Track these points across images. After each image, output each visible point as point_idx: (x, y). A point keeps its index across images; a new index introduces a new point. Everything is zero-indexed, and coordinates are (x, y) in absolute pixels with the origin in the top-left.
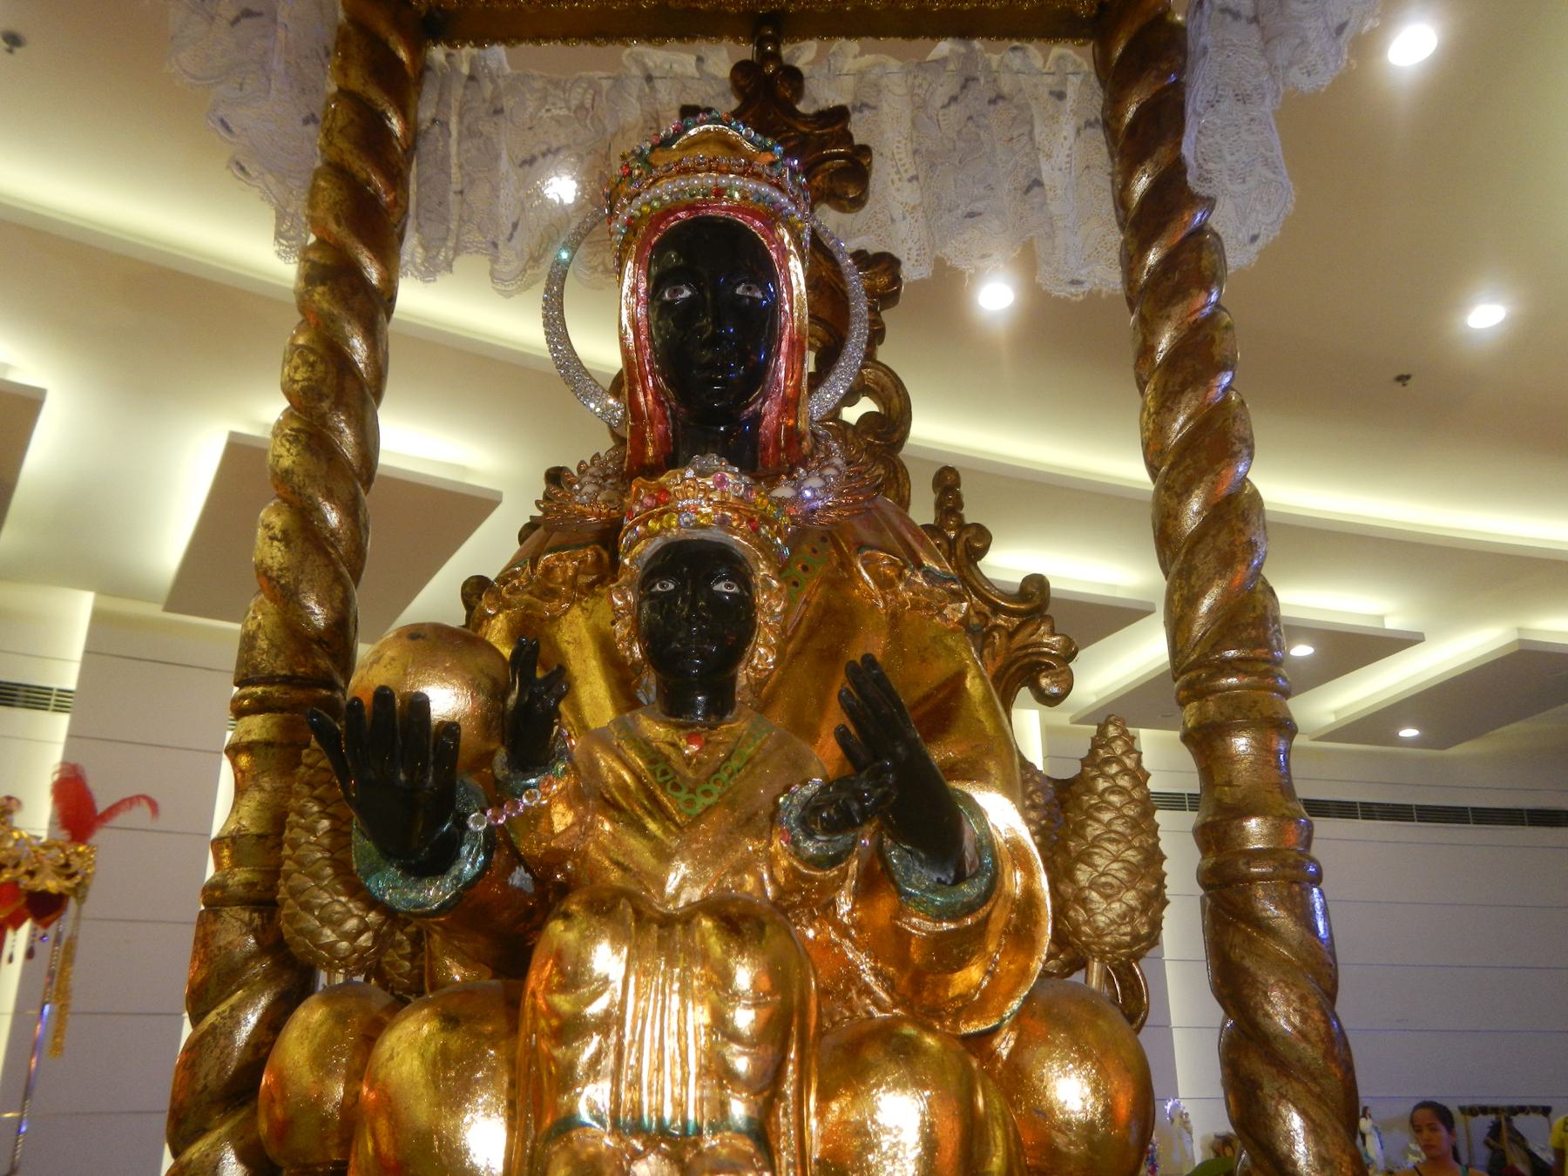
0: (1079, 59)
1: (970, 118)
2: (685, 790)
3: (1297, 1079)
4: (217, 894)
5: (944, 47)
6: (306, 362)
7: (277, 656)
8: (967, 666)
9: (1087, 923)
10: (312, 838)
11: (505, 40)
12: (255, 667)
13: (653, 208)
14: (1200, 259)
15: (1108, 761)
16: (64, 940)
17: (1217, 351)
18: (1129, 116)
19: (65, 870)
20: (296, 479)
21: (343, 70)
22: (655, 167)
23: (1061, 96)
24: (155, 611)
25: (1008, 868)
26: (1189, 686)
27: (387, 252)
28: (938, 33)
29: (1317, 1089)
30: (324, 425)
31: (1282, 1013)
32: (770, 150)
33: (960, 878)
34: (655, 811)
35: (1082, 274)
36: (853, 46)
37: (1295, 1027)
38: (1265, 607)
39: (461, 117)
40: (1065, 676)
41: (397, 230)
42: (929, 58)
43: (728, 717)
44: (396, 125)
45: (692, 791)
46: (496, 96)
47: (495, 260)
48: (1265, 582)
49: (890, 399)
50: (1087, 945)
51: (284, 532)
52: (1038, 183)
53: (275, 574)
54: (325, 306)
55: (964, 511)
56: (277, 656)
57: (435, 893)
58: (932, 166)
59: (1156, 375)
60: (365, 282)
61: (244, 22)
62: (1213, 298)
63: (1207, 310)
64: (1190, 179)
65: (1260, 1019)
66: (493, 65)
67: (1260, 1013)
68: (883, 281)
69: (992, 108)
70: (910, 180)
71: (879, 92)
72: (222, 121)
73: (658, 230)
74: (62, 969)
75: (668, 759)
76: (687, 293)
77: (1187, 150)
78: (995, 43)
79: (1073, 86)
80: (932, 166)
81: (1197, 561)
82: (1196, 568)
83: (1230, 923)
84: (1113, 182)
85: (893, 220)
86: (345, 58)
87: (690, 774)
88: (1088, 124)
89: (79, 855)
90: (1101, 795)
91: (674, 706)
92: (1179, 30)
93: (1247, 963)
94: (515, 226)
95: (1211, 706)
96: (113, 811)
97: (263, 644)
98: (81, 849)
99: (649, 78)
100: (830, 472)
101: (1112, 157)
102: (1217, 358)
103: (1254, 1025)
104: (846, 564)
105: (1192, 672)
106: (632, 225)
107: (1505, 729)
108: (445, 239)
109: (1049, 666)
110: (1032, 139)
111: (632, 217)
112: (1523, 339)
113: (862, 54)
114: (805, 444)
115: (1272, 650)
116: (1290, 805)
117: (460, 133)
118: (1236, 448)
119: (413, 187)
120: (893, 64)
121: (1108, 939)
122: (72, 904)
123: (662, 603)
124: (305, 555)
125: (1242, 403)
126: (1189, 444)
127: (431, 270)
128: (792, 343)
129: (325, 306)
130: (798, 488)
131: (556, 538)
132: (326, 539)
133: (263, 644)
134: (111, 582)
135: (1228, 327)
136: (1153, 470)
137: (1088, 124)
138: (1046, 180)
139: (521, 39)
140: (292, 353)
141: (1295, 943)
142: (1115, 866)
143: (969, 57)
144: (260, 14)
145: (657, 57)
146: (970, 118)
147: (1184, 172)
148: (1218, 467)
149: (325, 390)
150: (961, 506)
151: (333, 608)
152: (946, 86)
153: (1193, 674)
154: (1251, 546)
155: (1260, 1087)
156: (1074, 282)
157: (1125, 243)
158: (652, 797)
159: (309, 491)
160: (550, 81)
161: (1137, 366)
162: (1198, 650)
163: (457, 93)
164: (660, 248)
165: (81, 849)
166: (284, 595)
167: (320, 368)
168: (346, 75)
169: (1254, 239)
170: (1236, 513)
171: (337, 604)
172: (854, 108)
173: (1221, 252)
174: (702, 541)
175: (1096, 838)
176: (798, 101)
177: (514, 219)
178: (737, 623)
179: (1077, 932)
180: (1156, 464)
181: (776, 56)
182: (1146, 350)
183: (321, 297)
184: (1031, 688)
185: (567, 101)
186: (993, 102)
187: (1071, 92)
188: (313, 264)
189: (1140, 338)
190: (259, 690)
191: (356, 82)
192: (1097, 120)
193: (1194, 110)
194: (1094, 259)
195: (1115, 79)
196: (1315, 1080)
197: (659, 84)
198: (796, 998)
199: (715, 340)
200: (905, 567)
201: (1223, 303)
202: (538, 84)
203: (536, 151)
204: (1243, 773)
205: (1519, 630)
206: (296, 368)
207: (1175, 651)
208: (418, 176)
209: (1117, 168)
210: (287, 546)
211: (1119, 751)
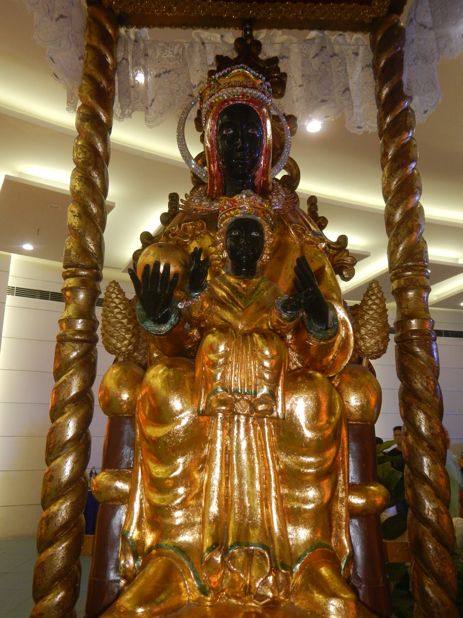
0: (364, 40)
1: (323, 63)
2: (244, 298)
3: (424, 403)
4: (63, 338)
5: (313, 34)
6: (83, 151)
7: (79, 257)
8: (326, 264)
9: (364, 345)
10: (113, 315)
11: (148, 26)
12: (71, 261)
13: (219, 99)
14: (406, 120)
15: (372, 295)
17: (411, 155)
18: (382, 64)
20: (82, 195)
21: (89, 36)
22: (220, 84)
23: (356, 54)
25: (341, 326)
26: (395, 274)
27: (109, 111)
28: (312, 29)
29: (430, 406)
30: (91, 175)
31: (419, 385)
33: (327, 328)
34: (234, 304)
35: (362, 125)
36: (280, 32)
37: (424, 386)
38: (423, 248)
39: (133, 57)
40: (352, 271)
42: (307, 38)
44: (109, 60)
45: (246, 298)
46: (145, 49)
47: (147, 113)
48: (423, 239)
49: (293, 170)
50: (363, 353)
51: (79, 214)
52: (348, 89)
53: (76, 229)
54: (89, 130)
55: (318, 212)
56: (79, 257)
57: (165, 328)
58: (309, 81)
59: (388, 164)
60: (102, 121)
61: (61, 20)
62: (410, 135)
63: (408, 139)
64: (405, 89)
66: (143, 36)
67: (413, 382)
69: (331, 58)
70: (300, 86)
71: (289, 51)
72: (51, 58)
75: (237, 288)
76: (231, 132)
77: (405, 78)
78: (332, 32)
79: (361, 50)
80: (309, 81)
81: (400, 231)
82: (399, 233)
83: (405, 354)
84: (375, 89)
85: (293, 102)
86: (90, 32)
87: (244, 293)
88: (367, 66)
90: (370, 306)
91: (237, 272)
92: (402, 30)
93: (410, 366)
94: (153, 101)
95: (402, 282)
97: (73, 253)
99: (203, 44)
100: (280, 196)
101: (375, 79)
102: (411, 157)
103: (411, 386)
104: (287, 229)
105: (396, 270)
108: (129, 106)
109: (346, 268)
110: (346, 72)
111: (212, 103)
113: (282, 35)
114: (270, 187)
115: (424, 262)
116: (427, 315)
117: (133, 63)
118: (416, 191)
120: (295, 40)
121: (370, 351)
123: (236, 239)
124: (86, 222)
125: (419, 174)
126: (399, 189)
128: (266, 151)
129: (89, 130)
131: (186, 218)
133: (73, 253)
135: (415, 146)
136: (386, 198)
137: (367, 66)
138: (351, 87)
139: (154, 26)
140: (77, 148)
141: (425, 360)
142: (373, 328)
143: (323, 39)
144: (66, 17)
145: (205, 34)
146: (323, 63)
147: (402, 86)
148: (410, 197)
149: (90, 162)
150: (317, 210)
151: (97, 241)
152: (314, 50)
153: (397, 271)
154: (419, 226)
155: (412, 406)
156: (359, 127)
157: (379, 114)
158: (233, 300)
159: (87, 199)
160: (166, 43)
161: (381, 160)
162: (399, 262)
163: (130, 47)
164: (221, 115)
166: (79, 236)
167: (88, 153)
168: (91, 39)
170: (414, 216)
171: (98, 240)
172: (280, 57)
173: (414, 116)
174: (247, 219)
175: (367, 319)
176: (259, 54)
177: (153, 98)
178: (257, 246)
179: (360, 349)
180: (387, 196)
181: (251, 36)
182: (385, 154)
183: (87, 126)
185: (172, 52)
186: (332, 56)
187: (360, 53)
188: (83, 114)
189: (383, 149)
191: (95, 42)
192: (370, 65)
193: (408, 64)
194: (365, 116)
195: (378, 48)
196: (429, 403)
197: (208, 47)
198: (284, 357)
199: (242, 149)
201: (414, 137)
202: (161, 44)
203: (161, 72)
204: (411, 304)
206: (79, 154)
207: (391, 262)
208: (118, 81)
209: (378, 84)
210: (80, 219)
211: (376, 292)
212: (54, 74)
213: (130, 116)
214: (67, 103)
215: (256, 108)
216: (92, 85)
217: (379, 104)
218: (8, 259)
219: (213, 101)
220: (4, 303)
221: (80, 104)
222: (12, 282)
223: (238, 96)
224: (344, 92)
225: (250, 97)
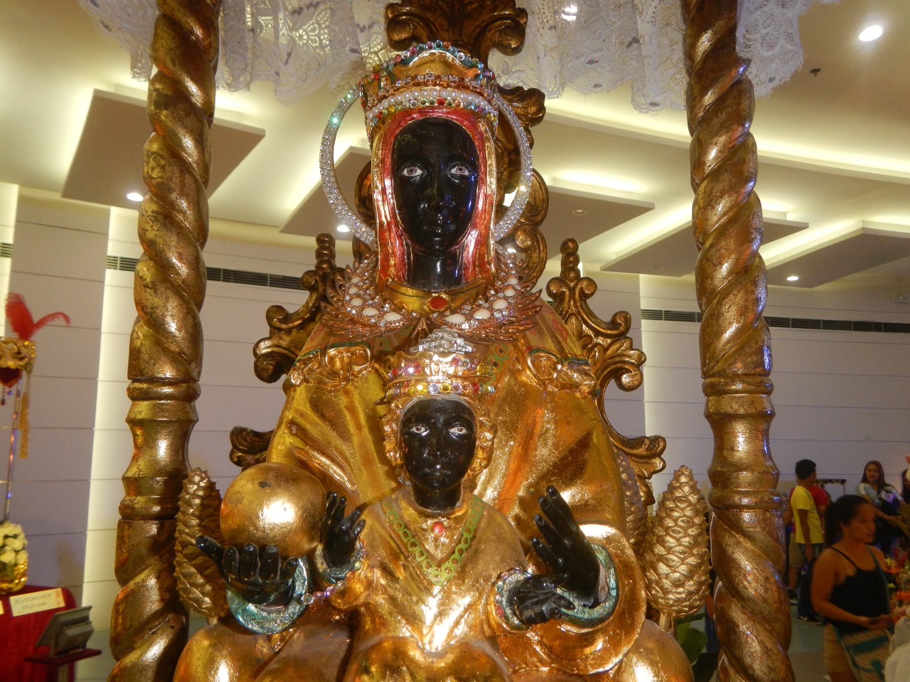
4: (128, 511)
6: (159, 165)
16: (22, 394)
19: (18, 355)
24: (57, 196)
32: (473, 66)
41: (212, 65)
43: (458, 504)
47: (277, 83)
52: (635, 40)
65: (740, 588)
67: (741, 585)
68: (533, 109)
70: (550, 28)
73: (399, 125)
74: (23, 411)
89: (25, 346)
94: (289, 55)
96: (42, 322)
98: (26, 343)
106: (381, 118)
107: (846, 277)
108: (245, 70)
112: (888, 48)
118: (753, 236)
119: (221, 34)
122: (24, 373)
127: (233, 86)
130: (491, 309)
132: (180, 286)
134: (29, 179)
165: (26, 343)
169: (771, 80)
184: (616, 381)
190: (145, 386)
200: (558, 363)
205: (863, 222)
206: (153, 169)
212: (102, 23)
213: (248, 86)
214: (132, 69)
215: (465, 125)
216: (173, 38)
217: (691, 68)
218: (107, 214)
219: (386, 112)
220: (103, 282)
221: (155, 70)
222: (114, 249)
223: (432, 103)
224: (630, 45)
225: (453, 105)
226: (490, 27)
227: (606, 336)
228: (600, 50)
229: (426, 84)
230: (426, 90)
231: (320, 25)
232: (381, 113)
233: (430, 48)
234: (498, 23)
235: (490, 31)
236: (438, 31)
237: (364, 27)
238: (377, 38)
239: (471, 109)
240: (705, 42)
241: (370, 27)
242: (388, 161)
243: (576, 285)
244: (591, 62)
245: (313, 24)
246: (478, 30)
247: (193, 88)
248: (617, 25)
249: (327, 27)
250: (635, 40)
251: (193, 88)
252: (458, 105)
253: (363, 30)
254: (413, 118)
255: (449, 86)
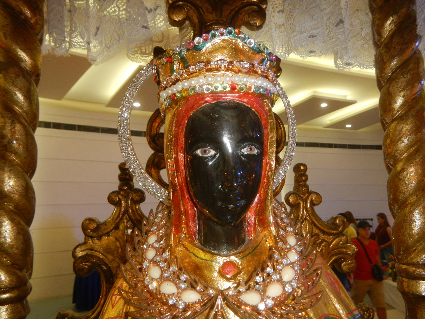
41: (39, 37)
52: (341, 21)
70: (279, 12)
226: (242, 11)
227: (329, 234)
228: (317, 28)
229: (218, 70)
230: (219, 76)
231: (119, 8)
232: (174, 95)
233: (222, 34)
234: (247, 8)
235: (241, 14)
236: (204, 13)
237: (151, 10)
238: (160, 17)
239: (260, 93)
240: (389, 25)
241: (155, 9)
242: (182, 139)
243: (308, 197)
244: (312, 36)
245: (114, 7)
246: (233, 13)
247: (23, 55)
248: (327, 11)
249: (124, 10)
250: (341, 21)
251: (23, 55)
252: (250, 88)
253: (150, 11)
254: (206, 102)
255: (240, 71)
